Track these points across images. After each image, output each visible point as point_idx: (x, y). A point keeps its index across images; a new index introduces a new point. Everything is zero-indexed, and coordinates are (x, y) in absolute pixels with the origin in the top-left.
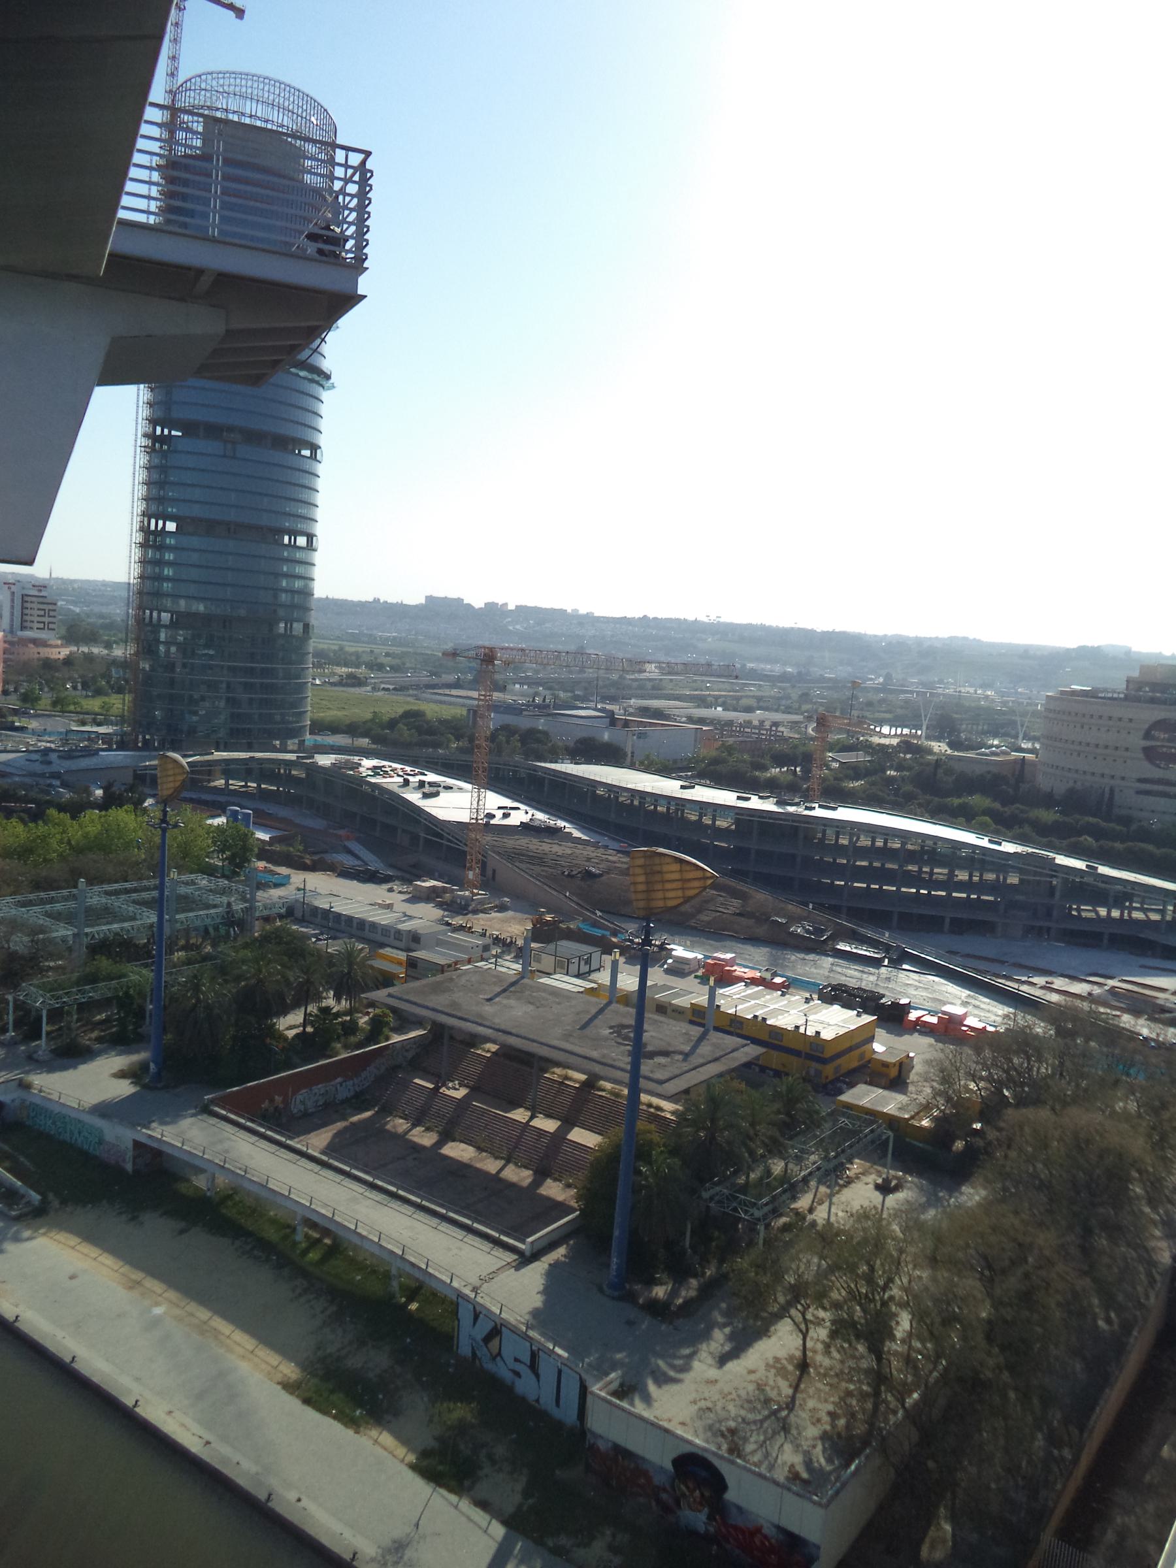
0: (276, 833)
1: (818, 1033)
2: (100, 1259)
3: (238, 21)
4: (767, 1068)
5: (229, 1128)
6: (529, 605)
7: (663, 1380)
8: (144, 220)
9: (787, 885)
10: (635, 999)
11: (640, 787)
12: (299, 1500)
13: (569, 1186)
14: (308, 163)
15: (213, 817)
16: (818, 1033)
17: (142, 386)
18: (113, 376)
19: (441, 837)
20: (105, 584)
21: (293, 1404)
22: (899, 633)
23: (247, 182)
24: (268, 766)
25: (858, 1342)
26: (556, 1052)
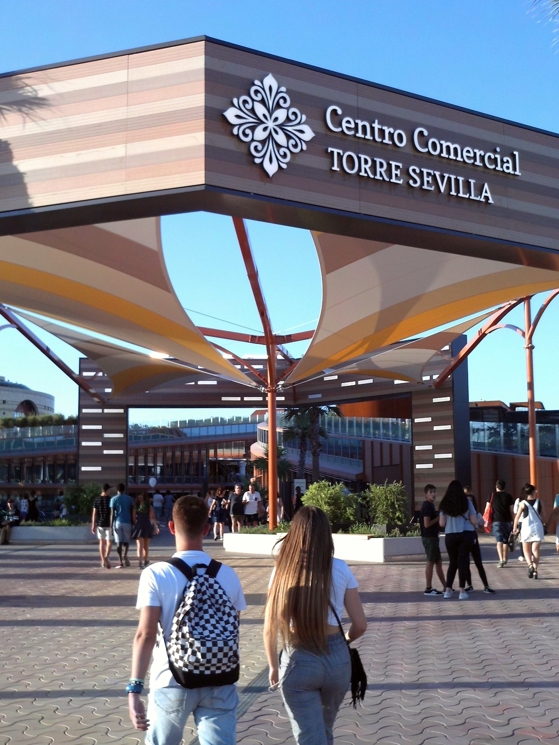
0: (471, 557)
1: (497, 531)
2: (151, 554)
3: (262, 130)
4: (520, 529)
5: (70, 634)
6: (247, 274)
7: (248, 527)
8: (441, 550)
9: (158, 432)
10: (81, 435)
11: (52, 210)
12: (4, 413)
13: (285, 410)
14: (302, 583)
15: (318, 422)
16: (497, 531)
17: (483, 562)
18: (287, 89)
19: (183, 700)
20: (172, 287)
21: (73, 528)
22: (154, 662)
23: (311, 596)
24: (320, 419)
25: (17, 589)
26: (21, 211)
